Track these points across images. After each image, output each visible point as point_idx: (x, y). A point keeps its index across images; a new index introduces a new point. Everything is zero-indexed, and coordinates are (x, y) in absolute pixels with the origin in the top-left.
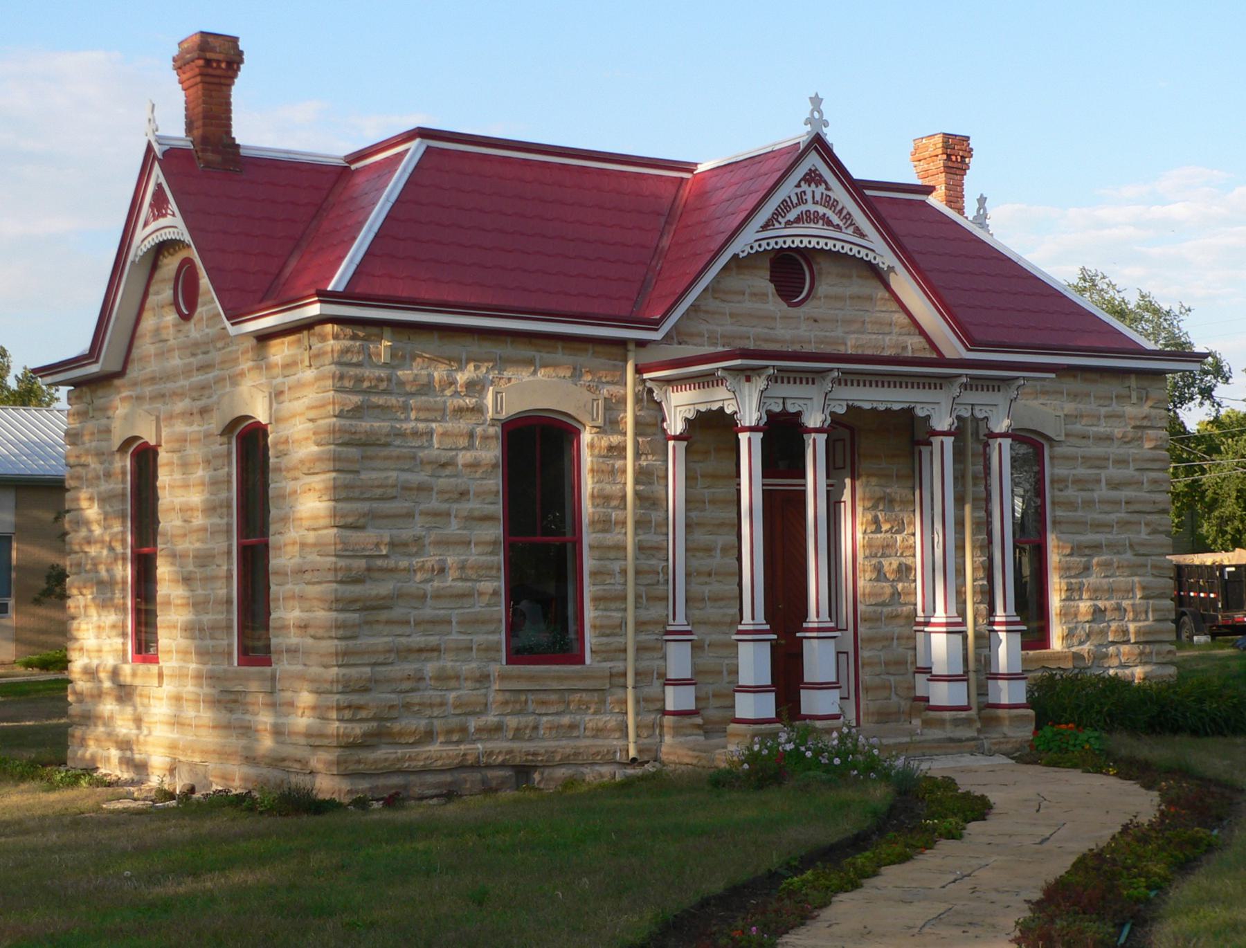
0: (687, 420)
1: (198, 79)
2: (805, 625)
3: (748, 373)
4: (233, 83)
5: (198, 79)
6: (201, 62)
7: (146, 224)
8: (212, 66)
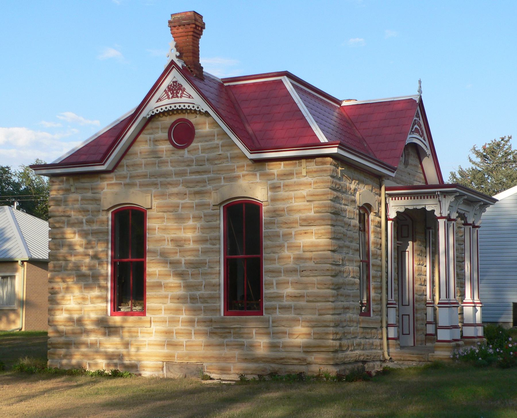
0: (398, 213)
1: (192, 33)
2: (464, 301)
3: (445, 194)
4: (200, 38)
5: (192, 33)
6: (194, 26)
7: (159, 100)
8: (189, 29)
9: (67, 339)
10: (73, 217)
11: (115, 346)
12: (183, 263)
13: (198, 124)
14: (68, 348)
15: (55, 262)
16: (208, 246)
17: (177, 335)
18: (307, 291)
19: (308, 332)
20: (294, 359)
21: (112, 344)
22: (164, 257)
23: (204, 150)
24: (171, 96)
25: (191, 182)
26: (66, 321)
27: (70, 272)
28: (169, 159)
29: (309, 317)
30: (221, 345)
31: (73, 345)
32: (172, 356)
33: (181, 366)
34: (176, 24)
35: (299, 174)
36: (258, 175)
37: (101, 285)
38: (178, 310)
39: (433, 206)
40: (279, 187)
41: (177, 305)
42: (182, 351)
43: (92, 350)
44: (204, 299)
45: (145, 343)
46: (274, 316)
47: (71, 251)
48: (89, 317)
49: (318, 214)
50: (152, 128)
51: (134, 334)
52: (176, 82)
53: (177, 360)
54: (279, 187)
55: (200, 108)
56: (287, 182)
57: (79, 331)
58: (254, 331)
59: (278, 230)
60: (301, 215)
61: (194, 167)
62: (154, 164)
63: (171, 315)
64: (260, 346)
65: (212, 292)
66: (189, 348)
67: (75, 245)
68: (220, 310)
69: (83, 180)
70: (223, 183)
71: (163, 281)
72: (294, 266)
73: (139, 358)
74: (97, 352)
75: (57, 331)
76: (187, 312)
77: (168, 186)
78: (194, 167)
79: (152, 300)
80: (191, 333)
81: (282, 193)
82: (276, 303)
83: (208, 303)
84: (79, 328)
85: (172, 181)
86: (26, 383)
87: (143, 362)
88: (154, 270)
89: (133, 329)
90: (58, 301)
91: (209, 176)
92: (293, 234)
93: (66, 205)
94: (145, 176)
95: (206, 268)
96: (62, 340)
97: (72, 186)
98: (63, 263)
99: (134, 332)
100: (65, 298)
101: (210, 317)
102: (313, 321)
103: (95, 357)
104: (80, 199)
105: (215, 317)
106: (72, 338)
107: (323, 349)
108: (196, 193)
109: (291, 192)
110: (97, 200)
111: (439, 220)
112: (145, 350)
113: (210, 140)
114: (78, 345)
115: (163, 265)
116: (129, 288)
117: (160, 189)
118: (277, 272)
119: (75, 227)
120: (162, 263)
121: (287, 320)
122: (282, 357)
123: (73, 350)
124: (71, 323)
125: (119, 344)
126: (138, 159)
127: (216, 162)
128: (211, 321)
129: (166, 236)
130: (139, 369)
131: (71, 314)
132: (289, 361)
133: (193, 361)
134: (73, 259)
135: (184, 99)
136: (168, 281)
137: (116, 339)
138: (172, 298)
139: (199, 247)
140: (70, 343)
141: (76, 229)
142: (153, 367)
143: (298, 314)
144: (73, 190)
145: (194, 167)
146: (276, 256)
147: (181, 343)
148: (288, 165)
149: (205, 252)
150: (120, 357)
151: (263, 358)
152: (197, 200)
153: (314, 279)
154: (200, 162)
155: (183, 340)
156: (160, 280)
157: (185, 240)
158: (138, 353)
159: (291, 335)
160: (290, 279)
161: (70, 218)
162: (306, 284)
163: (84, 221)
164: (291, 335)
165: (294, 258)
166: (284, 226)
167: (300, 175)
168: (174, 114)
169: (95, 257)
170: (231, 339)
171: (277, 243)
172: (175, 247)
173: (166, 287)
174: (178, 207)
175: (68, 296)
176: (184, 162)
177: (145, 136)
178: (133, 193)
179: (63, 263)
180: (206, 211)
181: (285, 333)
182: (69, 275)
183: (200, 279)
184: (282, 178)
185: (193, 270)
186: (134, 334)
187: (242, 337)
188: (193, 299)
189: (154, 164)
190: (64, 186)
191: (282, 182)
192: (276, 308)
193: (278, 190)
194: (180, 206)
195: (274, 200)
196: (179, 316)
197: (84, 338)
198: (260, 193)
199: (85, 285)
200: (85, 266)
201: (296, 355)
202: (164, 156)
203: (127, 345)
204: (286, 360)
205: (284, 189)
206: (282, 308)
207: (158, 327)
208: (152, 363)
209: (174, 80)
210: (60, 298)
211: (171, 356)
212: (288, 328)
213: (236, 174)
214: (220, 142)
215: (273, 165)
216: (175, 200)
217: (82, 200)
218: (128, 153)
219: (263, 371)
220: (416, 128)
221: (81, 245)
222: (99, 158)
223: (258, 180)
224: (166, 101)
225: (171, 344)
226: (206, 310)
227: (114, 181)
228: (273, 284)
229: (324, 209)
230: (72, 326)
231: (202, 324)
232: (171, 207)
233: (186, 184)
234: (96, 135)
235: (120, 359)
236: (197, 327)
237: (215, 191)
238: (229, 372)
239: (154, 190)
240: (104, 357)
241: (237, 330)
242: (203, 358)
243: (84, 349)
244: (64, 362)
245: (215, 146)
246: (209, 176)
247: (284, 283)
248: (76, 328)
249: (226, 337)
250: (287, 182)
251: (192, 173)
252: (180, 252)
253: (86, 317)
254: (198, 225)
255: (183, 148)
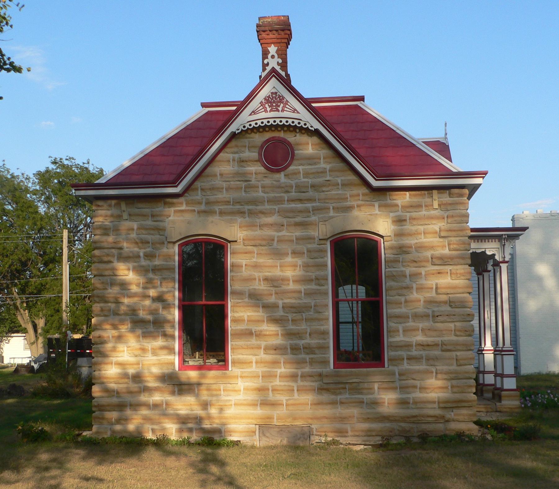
7: (254, 113)
9: (120, 400)
10: (126, 250)
11: (189, 407)
12: (281, 306)
13: (298, 144)
14: (121, 411)
15: (102, 305)
16: (313, 287)
17: (274, 392)
18: (442, 339)
19: (444, 386)
20: (431, 416)
21: (185, 405)
22: (255, 298)
23: (307, 174)
24: (268, 109)
25: (292, 211)
26: (119, 378)
27: (123, 317)
28: (260, 184)
29: (445, 368)
30: (333, 403)
31: (128, 407)
32: (270, 418)
33: (281, 429)
34: (267, 28)
35: (429, 206)
36: (377, 205)
37: (167, 333)
38: (275, 363)
39: (494, 250)
40: (405, 220)
41: (274, 356)
42: (282, 411)
43: (156, 412)
44: (309, 349)
45: (230, 403)
46: (400, 367)
47: (124, 291)
48: (151, 373)
49: (454, 252)
50: (237, 146)
51: (215, 393)
52: (276, 93)
53: (275, 422)
54: (405, 220)
55: (308, 125)
56: (414, 214)
57: (136, 389)
58: (376, 386)
59: (403, 269)
60: (432, 252)
61: (294, 193)
62: (238, 189)
63: (265, 369)
64: (384, 403)
65: (321, 341)
66: (291, 408)
67: (130, 284)
68: (329, 362)
69: (140, 205)
70: (332, 213)
71: (255, 328)
72: (426, 310)
73: (224, 421)
74: (165, 415)
75: (107, 390)
76: (288, 366)
77: (260, 215)
78: (294, 193)
79: (235, 350)
80: (293, 390)
81: (408, 227)
82: (403, 353)
83: (315, 354)
84: (136, 385)
85: (266, 209)
86: (95, 459)
87: (229, 426)
88: (239, 314)
89: (214, 387)
90: (107, 353)
91: (314, 204)
92: (423, 273)
93: (116, 235)
94: (228, 203)
95: (310, 313)
96: (115, 400)
97: (124, 211)
98: (113, 306)
99: (216, 390)
100: (118, 349)
101: (319, 370)
102: (451, 373)
103: (163, 421)
104: (135, 227)
105: (325, 370)
106: (128, 399)
107: (466, 404)
108: (297, 224)
109: (420, 227)
110: (160, 230)
111: (501, 264)
112: (230, 412)
113: (315, 164)
114: (136, 406)
115: (254, 309)
116: (206, 336)
117: (247, 219)
118: (403, 318)
119: (128, 262)
120: (253, 306)
121: (419, 372)
122: (414, 414)
123: (128, 412)
124: (126, 380)
125: (194, 405)
126: (218, 182)
127: (324, 189)
128: (320, 375)
129: (256, 274)
130: (223, 434)
131: (124, 369)
132: (423, 418)
133: (299, 423)
134: (126, 301)
135: (286, 114)
136: (260, 328)
137: (190, 399)
138: (266, 349)
139: (302, 288)
140: (124, 403)
141: (131, 265)
142: (244, 432)
143: (431, 365)
144: (125, 216)
145: (293, 194)
146: (403, 299)
147: (280, 402)
148: (415, 195)
149: (308, 294)
150: (199, 420)
151: (390, 416)
152: (298, 233)
153: (452, 325)
154: (300, 188)
155: (283, 398)
156: (250, 328)
157: (283, 280)
158: (222, 415)
159: (423, 389)
160: (421, 325)
161: (122, 251)
162: (441, 331)
163: (142, 254)
164: (423, 389)
165: (425, 302)
166: (411, 265)
167: (430, 208)
168: (267, 131)
169: (160, 299)
170: (345, 396)
171: (404, 284)
172: (269, 288)
173: (259, 335)
174: (273, 240)
175: (121, 347)
176: (279, 187)
177: (226, 154)
178: (212, 222)
179: (113, 306)
180: (310, 246)
181: (415, 387)
182: (122, 322)
183: (303, 326)
184: (408, 210)
185: (294, 315)
186: (215, 393)
187: (361, 393)
188: (295, 349)
189: (238, 189)
190: (115, 211)
191: (408, 215)
192: (403, 359)
193: (404, 223)
194: (276, 239)
195: (399, 235)
196: (276, 370)
197: (144, 398)
198: (382, 226)
199: (143, 333)
200: (143, 310)
201: (431, 412)
202: (253, 180)
203: (205, 405)
204: (419, 418)
205: (410, 223)
206: (410, 358)
207: (247, 384)
208: (241, 427)
209: (274, 91)
210: (110, 349)
211: (268, 418)
212: (419, 382)
213: (348, 204)
214: (328, 167)
215: (397, 195)
216: (268, 232)
217: (138, 229)
218: (203, 174)
219: (391, 432)
220: (304, 178)
221: (138, 285)
222: (172, 178)
223: (377, 212)
224: (263, 115)
225: (265, 403)
226: (312, 362)
227: (184, 207)
228: (398, 331)
229: (463, 246)
230: (126, 383)
231: (309, 378)
232: (264, 240)
233: (283, 213)
234: (142, 152)
235: (196, 423)
236: (300, 383)
237: (324, 223)
238: (346, 434)
239: (240, 220)
240: (176, 421)
241: (355, 384)
242: (311, 419)
243: (144, 412)
244: (118, 427)
245: (321, 170)
246: (314, 204)
247: (414, 330)
248: (134, 387)
249: (340, 393)
250: (414, 214)
251: (291, 200)
252: (276, 293)
253: (146, 373)
254: (299, 261)
255: (279, 171)
